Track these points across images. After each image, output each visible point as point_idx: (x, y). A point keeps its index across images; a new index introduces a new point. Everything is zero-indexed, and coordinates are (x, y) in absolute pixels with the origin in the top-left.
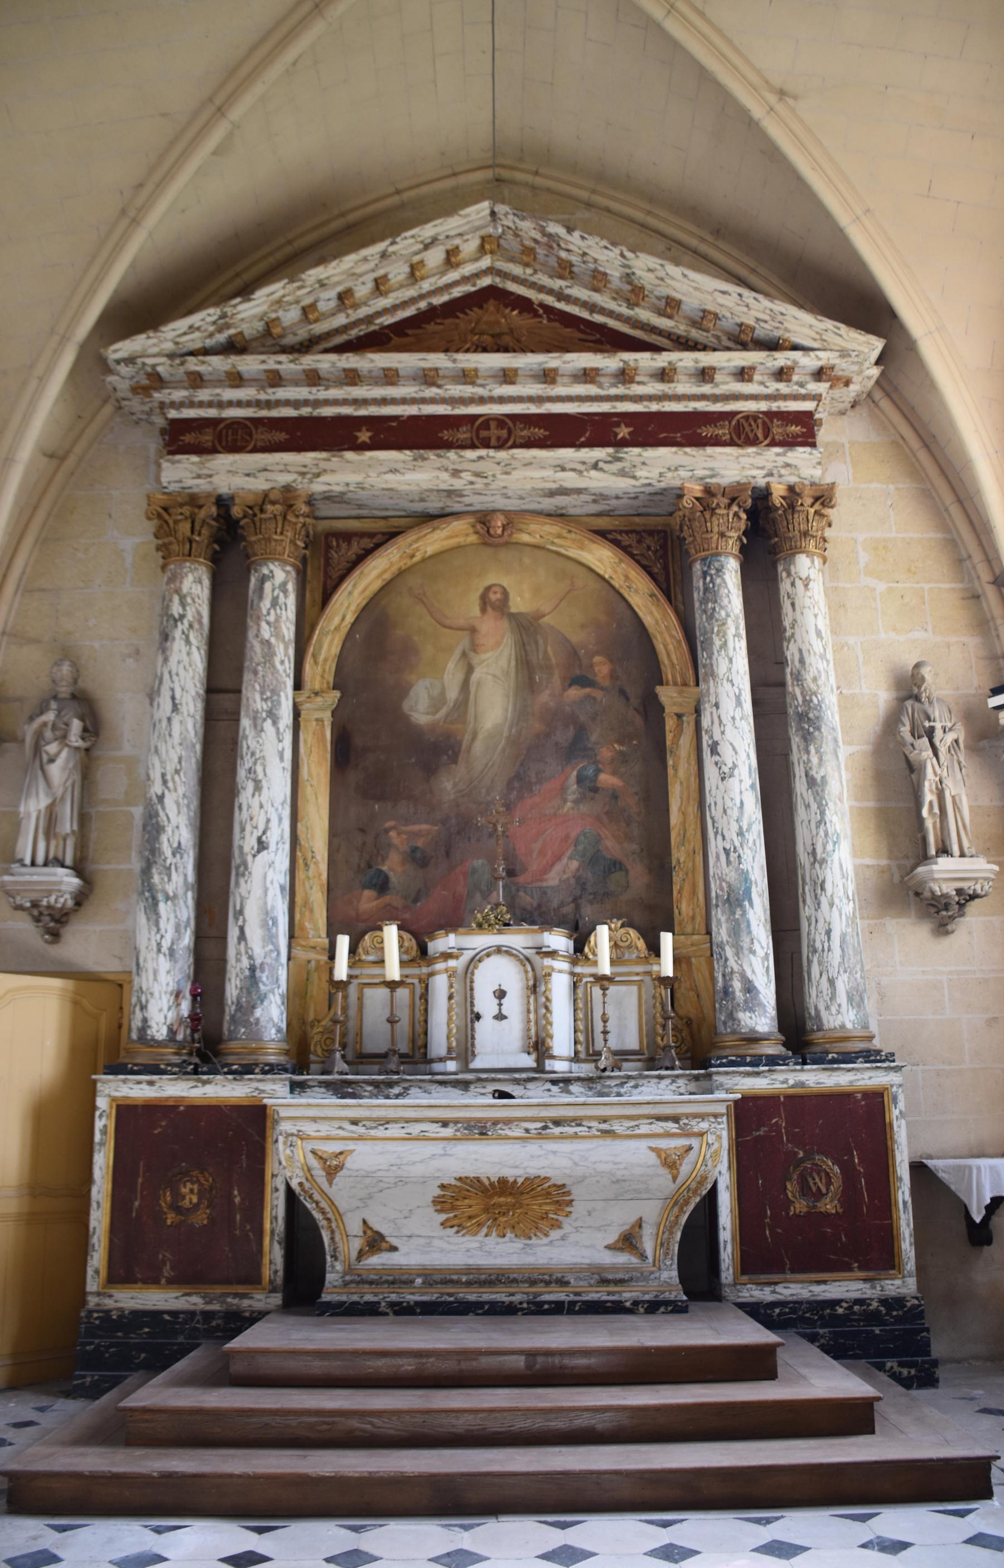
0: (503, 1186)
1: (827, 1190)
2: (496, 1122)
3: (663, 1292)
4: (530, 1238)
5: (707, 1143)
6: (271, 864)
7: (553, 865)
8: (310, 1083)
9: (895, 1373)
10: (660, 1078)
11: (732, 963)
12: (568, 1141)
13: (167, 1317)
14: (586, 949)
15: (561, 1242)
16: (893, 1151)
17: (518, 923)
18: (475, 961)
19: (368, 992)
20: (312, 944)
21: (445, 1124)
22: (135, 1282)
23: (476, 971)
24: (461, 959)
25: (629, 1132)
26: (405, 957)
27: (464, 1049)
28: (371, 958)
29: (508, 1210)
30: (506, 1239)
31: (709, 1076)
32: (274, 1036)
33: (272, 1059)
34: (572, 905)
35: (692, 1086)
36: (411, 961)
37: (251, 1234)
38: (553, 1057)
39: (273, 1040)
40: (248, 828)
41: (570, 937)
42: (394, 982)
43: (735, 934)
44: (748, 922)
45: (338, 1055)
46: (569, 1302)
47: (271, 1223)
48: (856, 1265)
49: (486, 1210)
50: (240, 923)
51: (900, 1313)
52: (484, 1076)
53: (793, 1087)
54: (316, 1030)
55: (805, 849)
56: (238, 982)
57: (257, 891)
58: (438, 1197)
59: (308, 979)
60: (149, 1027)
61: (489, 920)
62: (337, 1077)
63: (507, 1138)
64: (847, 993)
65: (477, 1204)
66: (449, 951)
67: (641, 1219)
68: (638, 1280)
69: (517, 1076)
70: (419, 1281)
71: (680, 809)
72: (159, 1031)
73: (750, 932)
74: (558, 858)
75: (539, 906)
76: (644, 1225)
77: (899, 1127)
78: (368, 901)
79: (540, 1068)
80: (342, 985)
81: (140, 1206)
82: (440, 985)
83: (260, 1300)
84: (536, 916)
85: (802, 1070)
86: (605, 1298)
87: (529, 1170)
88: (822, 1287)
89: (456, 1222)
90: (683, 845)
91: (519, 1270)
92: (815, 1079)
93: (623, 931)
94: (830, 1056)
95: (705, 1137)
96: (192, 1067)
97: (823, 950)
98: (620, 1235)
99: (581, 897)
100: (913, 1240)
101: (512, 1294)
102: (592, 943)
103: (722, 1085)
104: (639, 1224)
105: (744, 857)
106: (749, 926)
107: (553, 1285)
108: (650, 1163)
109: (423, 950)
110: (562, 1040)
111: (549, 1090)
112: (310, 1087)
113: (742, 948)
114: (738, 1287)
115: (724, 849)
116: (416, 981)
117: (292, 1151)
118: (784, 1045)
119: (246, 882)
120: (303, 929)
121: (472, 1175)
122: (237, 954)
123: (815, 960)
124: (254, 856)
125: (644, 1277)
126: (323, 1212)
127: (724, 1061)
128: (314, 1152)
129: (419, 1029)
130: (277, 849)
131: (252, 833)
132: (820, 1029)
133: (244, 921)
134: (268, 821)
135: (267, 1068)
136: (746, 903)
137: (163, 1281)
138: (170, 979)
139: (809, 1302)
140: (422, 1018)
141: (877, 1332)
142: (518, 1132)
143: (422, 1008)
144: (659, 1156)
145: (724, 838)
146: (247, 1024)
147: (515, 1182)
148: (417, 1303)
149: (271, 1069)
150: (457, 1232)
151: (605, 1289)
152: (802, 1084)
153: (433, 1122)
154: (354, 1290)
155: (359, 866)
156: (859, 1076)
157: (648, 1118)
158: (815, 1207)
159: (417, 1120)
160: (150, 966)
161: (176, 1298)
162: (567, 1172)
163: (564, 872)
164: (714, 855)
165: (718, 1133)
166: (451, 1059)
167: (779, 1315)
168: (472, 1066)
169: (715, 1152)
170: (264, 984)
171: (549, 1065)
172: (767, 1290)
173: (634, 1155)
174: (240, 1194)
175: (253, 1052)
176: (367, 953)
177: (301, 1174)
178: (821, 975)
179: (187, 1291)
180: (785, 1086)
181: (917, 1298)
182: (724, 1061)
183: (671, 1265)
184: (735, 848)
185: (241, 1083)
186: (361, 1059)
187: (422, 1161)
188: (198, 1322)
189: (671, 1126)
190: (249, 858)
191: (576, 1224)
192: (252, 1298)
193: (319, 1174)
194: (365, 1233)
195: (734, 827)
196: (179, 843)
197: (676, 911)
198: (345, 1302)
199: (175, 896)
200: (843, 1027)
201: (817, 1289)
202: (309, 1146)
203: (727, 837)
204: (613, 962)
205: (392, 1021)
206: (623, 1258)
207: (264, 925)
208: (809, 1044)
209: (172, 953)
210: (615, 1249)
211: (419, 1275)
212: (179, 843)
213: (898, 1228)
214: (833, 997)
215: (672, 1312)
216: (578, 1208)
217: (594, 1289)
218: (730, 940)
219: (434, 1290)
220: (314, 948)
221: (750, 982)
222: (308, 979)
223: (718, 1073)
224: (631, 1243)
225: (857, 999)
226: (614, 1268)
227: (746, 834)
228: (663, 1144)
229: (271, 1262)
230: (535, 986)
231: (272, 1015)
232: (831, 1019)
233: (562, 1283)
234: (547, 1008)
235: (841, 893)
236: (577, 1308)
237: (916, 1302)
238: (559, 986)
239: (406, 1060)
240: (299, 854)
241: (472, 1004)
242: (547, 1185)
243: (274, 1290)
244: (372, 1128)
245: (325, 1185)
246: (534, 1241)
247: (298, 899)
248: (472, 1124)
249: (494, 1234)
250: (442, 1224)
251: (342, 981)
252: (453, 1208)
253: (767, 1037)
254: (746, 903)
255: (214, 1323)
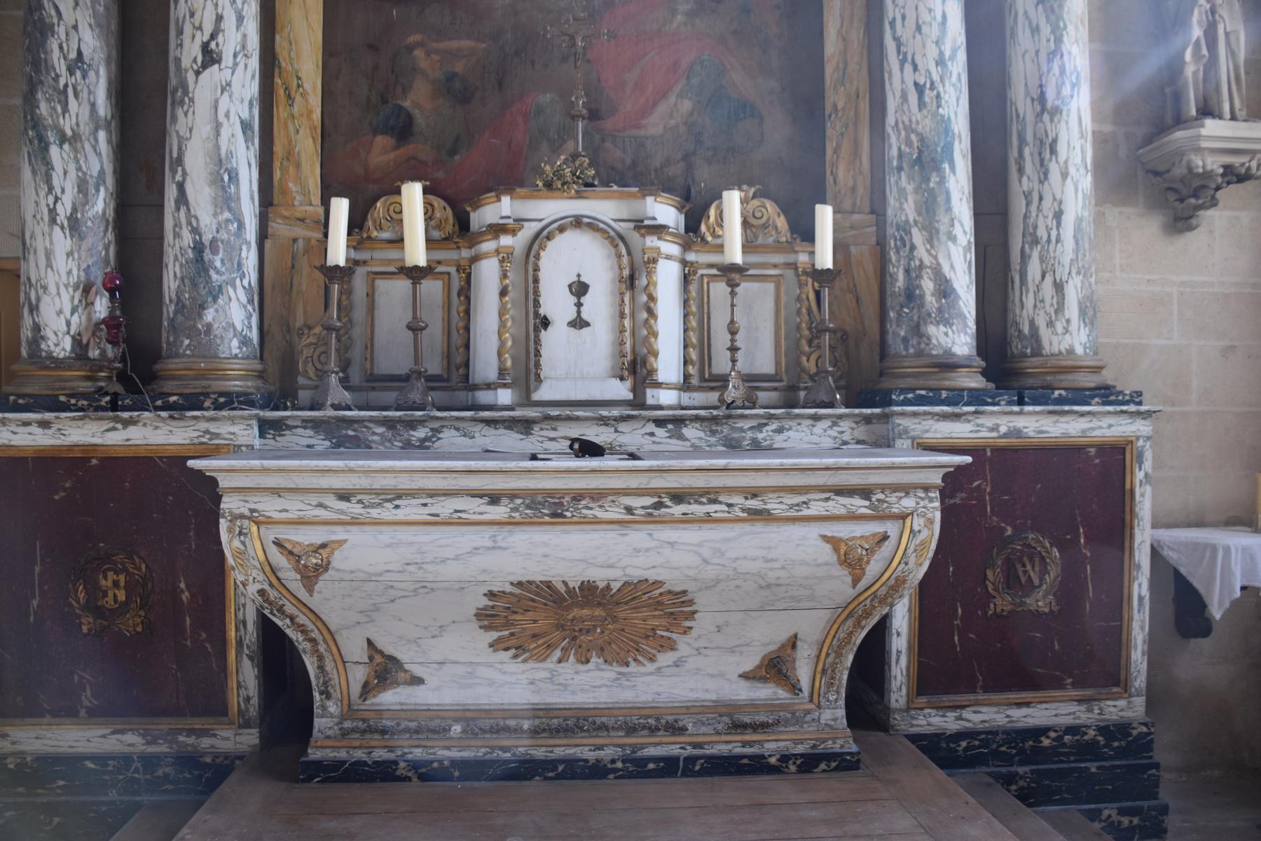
0: (589, 593)
1: (1041, 580)
2: (578, 496)
3: (825, 741)
4: (627, 664)
5: (912, 530)
6: (226, 87)
7: (655, 105)
8: (290, 422)
9: (1113, 822)
10: (816, 418)
11: (921, 252)
12: (696, 526)
13: (90, 765)
14: (703, 228)
15: (675, 670)
16: (1132, 528)
17: (606, 184)
18: (542, 238)
19: (382, 285)
20: (298, 215)
21: (494, 499)
22: (41, 715)
23: (542, 253)
24: (520, 234)
25: (793, 513)
26: (436, 234)
27: (525, 370)
28: (386, 235)
29: (595, 627)
30: (591, 666)
31: (886, 417)
32: (236, 351)
33: (235, 385)
34: (682, 164)
35: (861, 432)
36: (445, 239)
37: (208, 645)
38: (658, 385)
39: (236, 356)
40: (188, 29)
41: (680, 209)
42: (416, 268)
43: (927, 211)
44: (948, 194)
45: (334, 379)
46: (686, 759)
47: (237, 630)
48: (1070, 680)
49: (560, 627)
50: (178, 178)
51: (1123, 743)
52: (554, 412)
53: (1005, 436)
54: (305, 341)
55: (1027, 93)
56: (177, 269)
57: (203, 129)
58: (485, 609)
59: (293, 267)
60: (43, 338)
61: (564, 176)
62: (331, 413)
63: (597, 522)
64: (1080, 303)
65: (546, 618)
66: (501, 222)
67: (796, 636)
68: (787, 723)
69: (605, 413)
70: (457, 728)
71: (839, 32)
72: (59, 344)
73: (949, 209)
74: (663, 95)
75: (635, 163)
76: (798, 643)
77: (1143, 495)
78: (381, 151)
79: (638, 402)
80: (334, 273)
81: (38, 606)
82: (488, 273)
83: (227, 739)
84: (632, 176)
85: (1021, 413)
86: (739, 750)
87: (629, 571)
88: (1024, 711)
89: (514, 642)
90: (843, 84)
91: (609, 710)
92: (1038, 425)
93: (756, 202)
94: (1057, 393)
95: (908, 521)
96: (108, 398)
97: (1049, 241)
98: (763, 658)
99: (694, 153)
100: (1146, 648)
101: (600, 748)
102: (712, 219)
103: (906, 431)
104: (793, 642)
105: (945, 97)
106: (948, 200)
107: (661, 733)
108: (821, 561)
109: (463, 224)
110: (668, 365)
111: (652, 434)
112: (290, 428)
113: (937, 231)
114: (913, 712)
115: (916, 84)
116: (453, 270)
117: (243, 543)
118: (985, 373)
119: (186, 114)
120: (285, 192)
121: (538, 578)
122: (176, 225)
123: (1035, 255)
124: (198, 73)
125: (797, 719)
126: (303, 630)
127: (910, 396)
128: (278, 544)
129: (457, 340)
130: (236, 64)
131: (194, 36)
132: (1037, 351)
133: (185, 174)
134: (219, 18)
135: (222, 400)
136: (946, 166)
137: (83, 713)
138: (72, 265)
139: (1007, 732)
140: (461, 324)
141: (1094, 770)
142: (615, 513)
143: (462, 308)
144: (836, 550)
145: (915, 68)
146: (193, 333)
147: (608, 587)
148: (454, 763)
149: (229, 401)
150: (515, 656)
151: (739, 738)
152: (1017, 433)
153: (473, 496)
154: (357, 743)
155: (368, 101)
156: (1095, 423)
157: (823, 491)
158: (1022, 604)
159: (448, 494)
160: (40, 244)
161: (104, 736)
162: (691, 573)
163: (671, 116)
164: (898, 94)
165: (930, 515)
166: (505, 386)
167: (966, 749)
168: (536, 397)
169: (922, 543)
170: (218, 272)
171: (653, 396)
172: (951, 715)
173: (799, 548)
174: (188, 587)
175: (202, 375)
176: (380, 228)
177: (261, 577)
178: (1043, 277)
179: (119, 727)
180: (994, 434)
181: (1145, 724)
182: (910, 396)
183: (836, 700)
184: (932, 83)
185: (181, 423)
186: (374, 385)
187: (457, 558)
188: (136, 771)
189: (858, 504)
190: (191, 77)
191: (696, 645)
192: (215, 735)
193: (291, 577)
194: (371, 658)
195: (932, 52)
196: (80, 53)
197: (829, 178)
198: (344, 762)
199: (76, 137)
200: (1071, 351)
201: (1017, 713)
202: (271, 534)
203: (920, 67)
204: (747, 247)
205: (415, 328)
206: (766, 692)
207: (216, 180)
208: (1018, 374)
209: (74, 225)
210: (754, 678)
211: (456, 720)
212: (80, 53)
213: (1129, 634)
214: (1060, 308)
215: (836, 769)
216: (703, 623)
217: (724, 738)
218: (920, 219)
219: (480, 743)
220: (302, 220)
221: (947, 281)
222: (293, 267)
223: (903, 414)
224: (780, 671)
225: (1091, 313)
226: (753, 706)
227: (949, 64)
228: (844, 531)
229: (239, 686)
230: (632, 278)
231: (233, 317)
232: (1055, 340)
233: (675, 729)
234: (651, 312)
235: (1078, 160)
236: (697, 768)
237: (1145, 729)
238: (667, 277)
239: (439, 387)
240: (278, 81)
241: (537, 304)
242: (657, 592)
243: (247, 724)
244: (373, 506)
245: (302, 594)
246: (633, 667)
247: (278, 148)
248: (540, 498)
249: (572, 658)
250: (491, 646)
251: (337, 267)
252: (507, 624)
253: (967, 363)
254: (946, 166)
255: (160, 772)
